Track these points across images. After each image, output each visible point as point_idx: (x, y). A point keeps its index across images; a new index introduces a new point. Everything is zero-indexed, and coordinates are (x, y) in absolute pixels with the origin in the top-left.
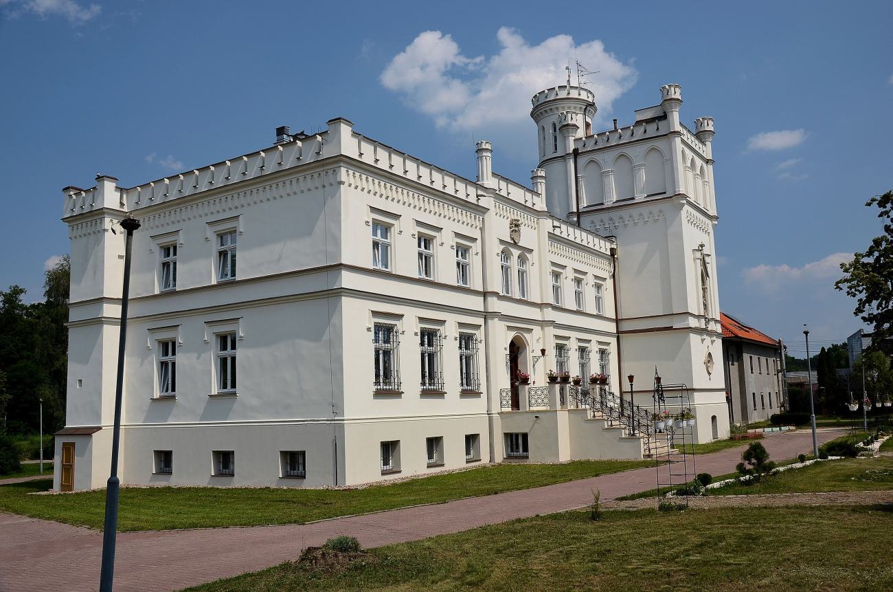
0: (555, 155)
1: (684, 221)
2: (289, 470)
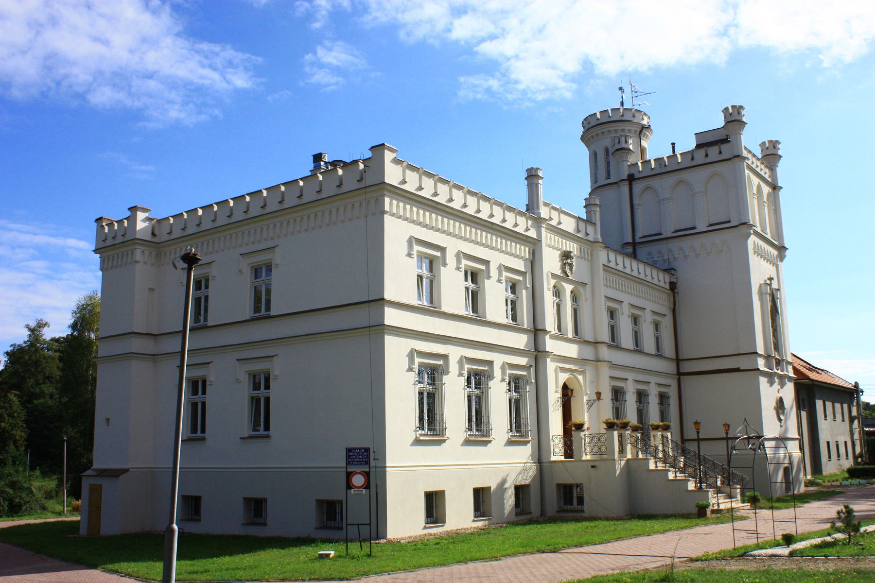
0: (609, 181)
2: (325, 520)
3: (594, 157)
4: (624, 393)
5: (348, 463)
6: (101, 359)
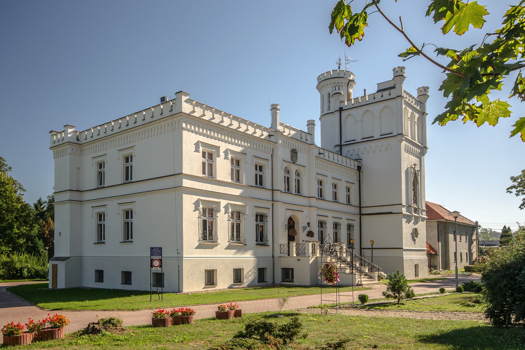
1: (403, 150)
3: (322, 97)
4: (326, 224)
5: (151, 255)
6: (56, 203)
